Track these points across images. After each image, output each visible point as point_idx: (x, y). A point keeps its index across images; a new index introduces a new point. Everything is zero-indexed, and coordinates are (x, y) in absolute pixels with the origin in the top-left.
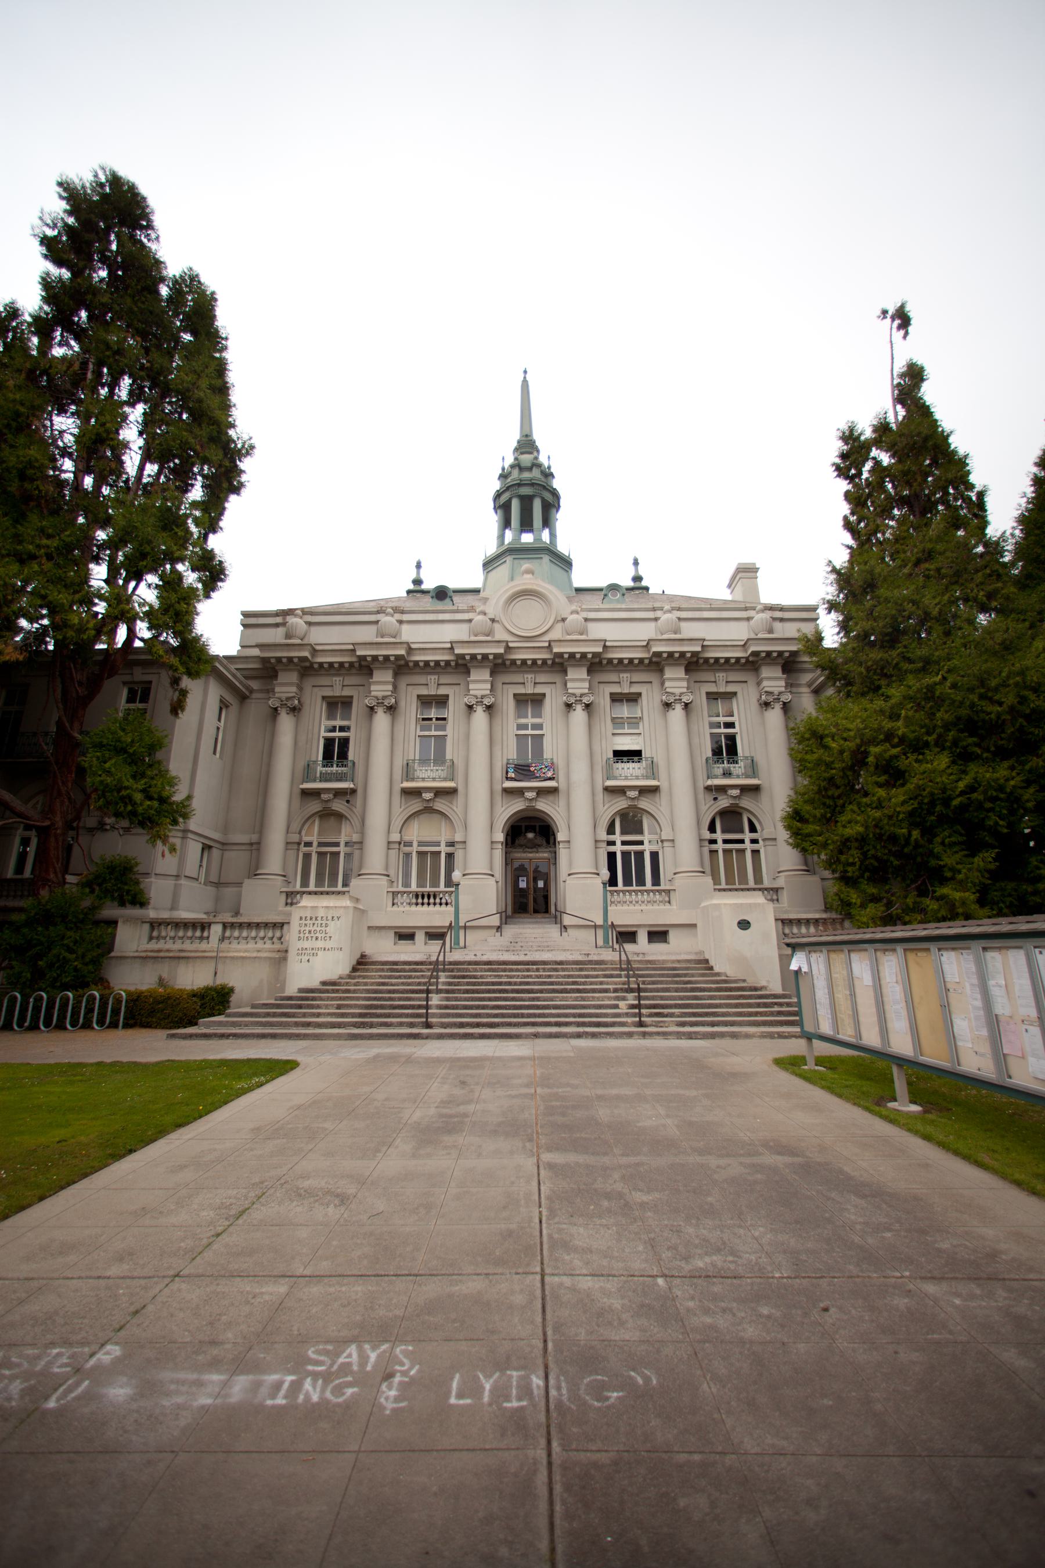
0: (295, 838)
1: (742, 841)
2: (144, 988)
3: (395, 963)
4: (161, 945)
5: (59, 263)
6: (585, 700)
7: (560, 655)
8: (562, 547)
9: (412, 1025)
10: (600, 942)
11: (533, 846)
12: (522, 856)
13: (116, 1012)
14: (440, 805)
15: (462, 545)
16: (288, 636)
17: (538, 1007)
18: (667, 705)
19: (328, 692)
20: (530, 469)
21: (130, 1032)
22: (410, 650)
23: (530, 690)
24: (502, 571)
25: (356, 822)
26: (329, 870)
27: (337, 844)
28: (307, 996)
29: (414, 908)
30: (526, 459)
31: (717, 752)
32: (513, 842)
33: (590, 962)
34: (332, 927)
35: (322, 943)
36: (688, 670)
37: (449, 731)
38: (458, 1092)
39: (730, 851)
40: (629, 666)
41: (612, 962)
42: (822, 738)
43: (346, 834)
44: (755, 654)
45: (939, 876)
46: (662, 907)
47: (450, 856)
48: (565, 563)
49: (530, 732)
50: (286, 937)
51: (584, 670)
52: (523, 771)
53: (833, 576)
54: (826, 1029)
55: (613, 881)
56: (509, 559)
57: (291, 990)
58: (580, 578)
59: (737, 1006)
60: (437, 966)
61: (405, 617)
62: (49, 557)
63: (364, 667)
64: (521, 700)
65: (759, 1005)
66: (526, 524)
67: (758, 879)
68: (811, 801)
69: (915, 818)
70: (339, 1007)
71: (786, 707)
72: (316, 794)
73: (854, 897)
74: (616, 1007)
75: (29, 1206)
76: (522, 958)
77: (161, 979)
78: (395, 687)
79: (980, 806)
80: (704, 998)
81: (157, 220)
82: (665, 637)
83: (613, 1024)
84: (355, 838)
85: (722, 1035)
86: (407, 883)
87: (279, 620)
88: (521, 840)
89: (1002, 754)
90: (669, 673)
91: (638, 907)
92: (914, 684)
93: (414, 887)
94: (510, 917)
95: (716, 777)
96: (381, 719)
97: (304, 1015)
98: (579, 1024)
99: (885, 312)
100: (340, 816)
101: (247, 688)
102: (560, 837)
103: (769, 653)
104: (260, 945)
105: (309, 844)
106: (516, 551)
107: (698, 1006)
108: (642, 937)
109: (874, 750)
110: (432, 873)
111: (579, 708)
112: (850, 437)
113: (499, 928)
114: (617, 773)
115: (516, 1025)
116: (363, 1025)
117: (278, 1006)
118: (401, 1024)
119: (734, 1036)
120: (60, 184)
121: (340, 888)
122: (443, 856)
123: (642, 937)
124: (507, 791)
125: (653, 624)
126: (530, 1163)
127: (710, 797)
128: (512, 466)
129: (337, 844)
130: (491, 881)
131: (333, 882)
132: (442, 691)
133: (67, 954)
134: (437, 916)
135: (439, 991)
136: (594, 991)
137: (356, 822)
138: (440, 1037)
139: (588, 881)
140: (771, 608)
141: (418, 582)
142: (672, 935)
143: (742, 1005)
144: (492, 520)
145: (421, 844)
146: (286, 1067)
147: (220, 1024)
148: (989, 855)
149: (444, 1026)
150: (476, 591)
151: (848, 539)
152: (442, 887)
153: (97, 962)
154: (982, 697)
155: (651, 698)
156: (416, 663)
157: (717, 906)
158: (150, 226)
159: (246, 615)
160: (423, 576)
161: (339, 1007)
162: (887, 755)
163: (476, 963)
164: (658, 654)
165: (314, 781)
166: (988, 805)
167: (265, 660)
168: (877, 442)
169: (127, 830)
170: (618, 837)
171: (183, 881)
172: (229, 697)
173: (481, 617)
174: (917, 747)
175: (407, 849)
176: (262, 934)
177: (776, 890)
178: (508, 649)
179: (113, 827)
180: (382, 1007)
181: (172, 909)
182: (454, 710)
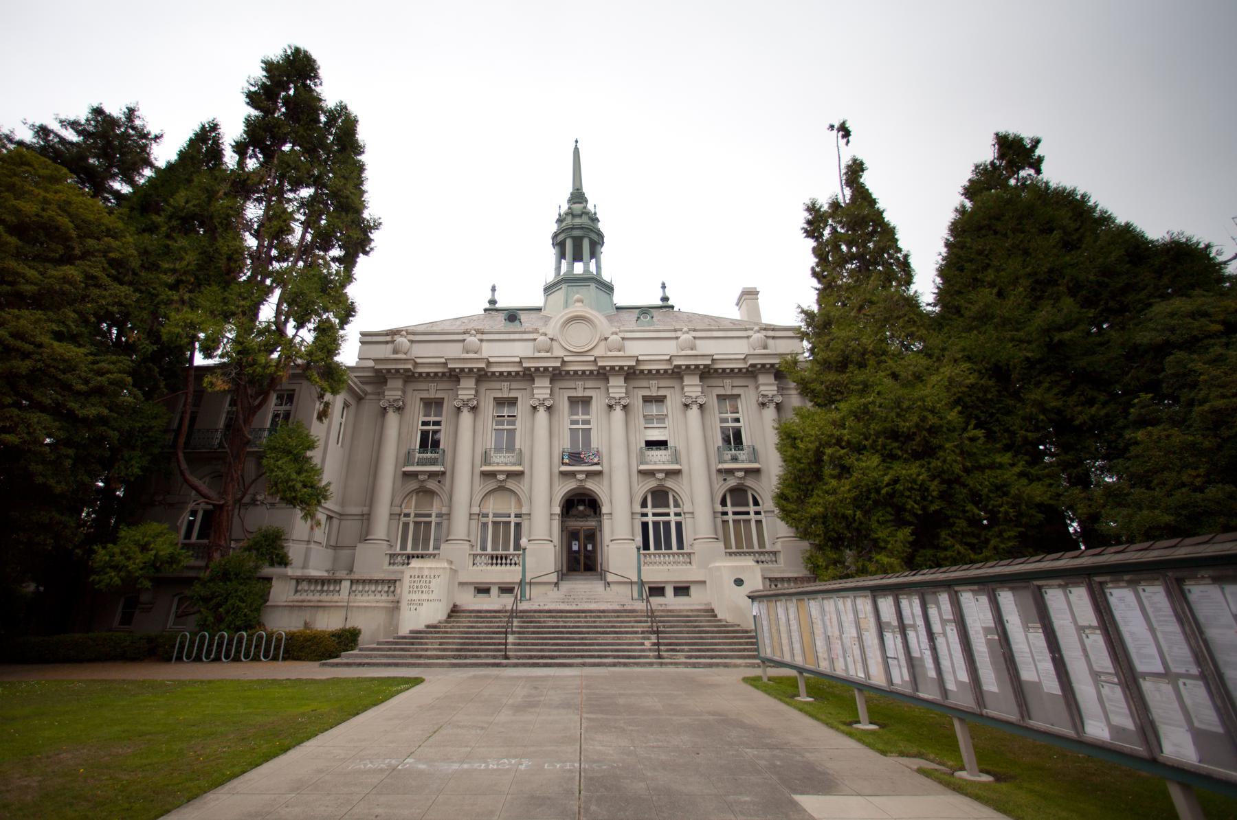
0: (397, 510)
1: (668, 515)
2: (294, 630)
3: (480, 611)
4: (304, 597)
5: (256, 108)
6: (623, 402)
7: (604, 368)
8: (606, 276)
9: (494, 657)
10: (636, 595)
11: (584, 516)
12: (575, 524)
13: (277, 647)
14: (511, 484)
15: (528, 273)
16: (395, 352)
17: (585, 644)
18: (687, 406)
19: (425, 395)
20: (580, 216)
21: (287, 663)
22: (489, 363)
23: (432, 395)
24: (559, 296)
25: (445, 498)
26: (421, 537)
27: (430, 515)
28: (416, 637)
29: (489, 567)
30: (577, 207)
31: (727, 440)
32: (567, 513)
33: (625, 611)
34: (434, 583)
35: (427, 595)
36: (701, 378)
37: (518, 425)
38: (533, 692)
39: (739, 521)
40: (657, 375)
41: (642, 611)
42: (795, 439)
43: (436, 508)
44: (753, 366)
45: (877, 546)
46: (684, 567)
47: (518, 525)
48: (608, 288)
49: (580, 426)
50: (398, 591)
51: (622, 379)
52: (575, 458)
53: (803, 316)
54: (787, 659)
55: (646, 546)
56: (564, 286)
57: (404, 630)
58: (620, 299)
59: (731, 644)
60: (513, 614)
61: (485, 337)
62: (244, 313)
63: (453, 376)
64: (573, 401)
65: (747, 644)
66: (577, 257)
67: (761, 543)
68: (788, 486)
69: (857, 502)
70: (441, 644)
71: (778, 407)
72: (415, 475)
73: (821, 562)
74: (643, 644)
75: (261, 764)
76: (574, 607)
77: (306, 623)
78: (477, 391)
79: (902, 494)
80: (710, 639)
81: (321, 72)
82: (684, 353)
83: (640, 657)
84: (444, 510)
85: (717, 665)
86: (484, 548)
87: (388, 338)
88: (573, 512)
89: (916, 456)
90: (688, 380)
91: (665, 567)
92: (855, 402)
93: (489, 551)
94: (566, 575)
95: (725, 462)
96: (466, 417)
97: (416, 650)
98: (615, 657)
99: (832, 127)
100: (431, 493)
101: (363, 391)
102: (605, 510)
103: (763, 365)
104: (378, 597)
105: (407, 515)
106: (571, 280)
107: (702, 644)
108: (669, 591)
109: (829, 451)
110: (504, 539)
111: (618, 408)
112: (812, 208)
113: (556, 584)
114: (648, 459)
115: (569, 657)
116: (460, 657)
117: (397, 643)
118: (487, 657)
119: (726, 665)
120: (263, 62)
121: (431, 551)
122: (512, 525)
123: (669, 591)
124: (563, 474)
125: (674, 342)
126: (577, 718)
127: (721, 478)
128: (567, 214)
129: (430, 515)
130: (551, 546)
131: (426, 546)
132: (513, 394)
133: (238, 603)
134: (508, 574)
135: (513, 633)
136: (627, 633)
137: (445, 498)
138: (516, 665)
139: (626, 546)
140: (766, 328)
141: (493, 302)
142: (693, 590)
143: (735, 644)
144: (551, 253)
145: (495, 515)
146: (418, 681)
147: (356, 656)
148: (908, 531)
149: (518, 657)
150: (539, 309)
151: (815, 283)
152: (512, 551)
153: (258, 610)
154: (898, 415)
155: (674, 400)
156: (493, 373)
157: (718, 568)
158: (316, 76)
159: (363, 334)
160: (497, 297)
161: (441, 644)
162: (838, 454)
163: (540, 611)
164: (679, 367)
165: (413, 465)
166: (907, 493)
167: (378, 371)
168: (832, 215)
169: (273, 505)
170: (650, 510)
171: (313, 546)
172: (350, 400)
173: (542, 338)
174: (859, 449)
175: (485, 520)
176: (380, 588)
177: (775, 553)
178: (564, 362)
179: (262, 503)
180: (472, 644)
181: (304, 567)
182: (522, 409)
